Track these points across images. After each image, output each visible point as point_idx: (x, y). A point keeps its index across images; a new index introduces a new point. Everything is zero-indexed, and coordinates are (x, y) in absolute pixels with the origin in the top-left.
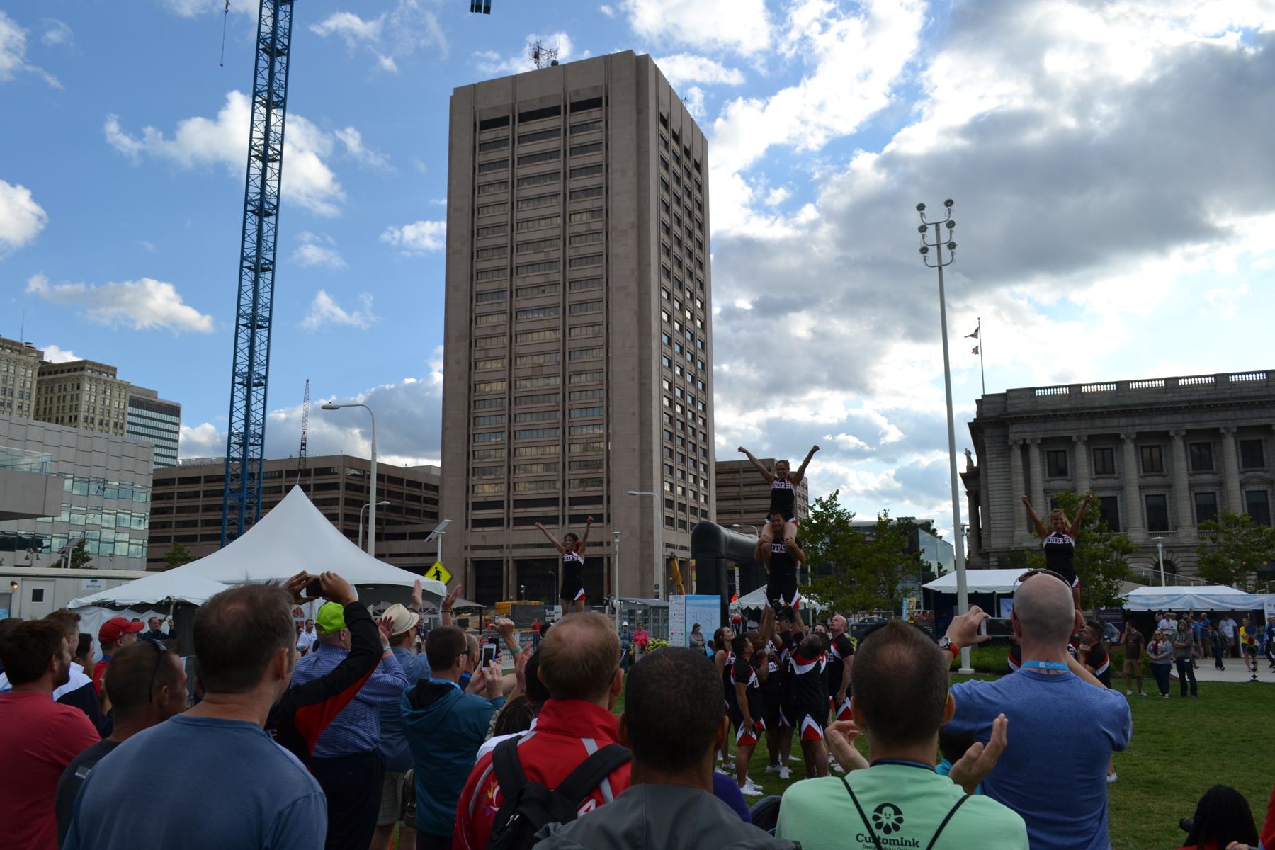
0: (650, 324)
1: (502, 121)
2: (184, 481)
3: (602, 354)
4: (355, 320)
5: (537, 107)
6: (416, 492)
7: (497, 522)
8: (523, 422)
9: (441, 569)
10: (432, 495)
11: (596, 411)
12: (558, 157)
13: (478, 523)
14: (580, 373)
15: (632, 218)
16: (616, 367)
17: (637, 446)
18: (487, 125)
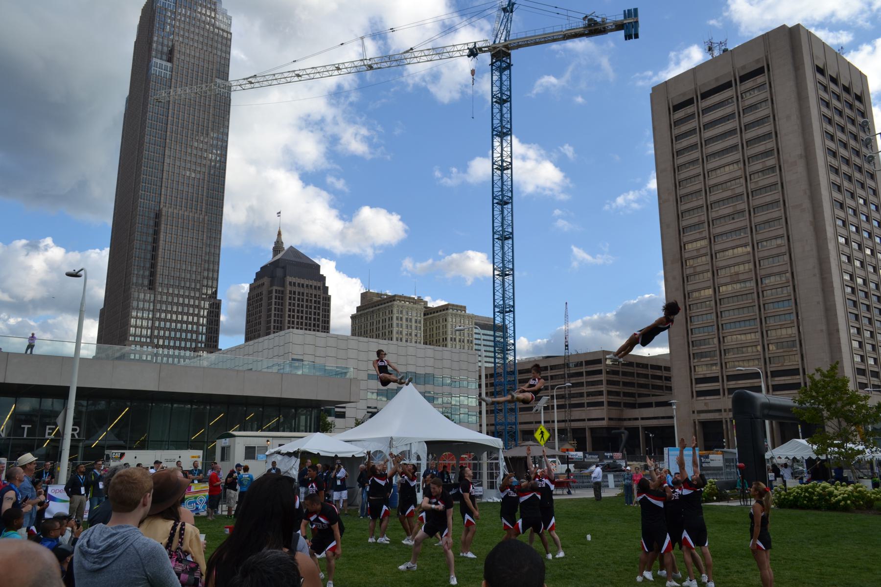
0: (825, 231)
1: (690, 102)
2: (588, 363)
3: (786, 258)
4: (599, 260)
5: (714, 85)
6: (658, 373)
7: (715, 392)
8: (727, 317)
9: (544, 430)
10: (665, 374)
11: (786, 303)
12: (734, 118)
13: (701, 394)
14: (770, 275)
15: (799, 151)
16: (799, 268)
17: (824, 328)
18: (677, 108)
